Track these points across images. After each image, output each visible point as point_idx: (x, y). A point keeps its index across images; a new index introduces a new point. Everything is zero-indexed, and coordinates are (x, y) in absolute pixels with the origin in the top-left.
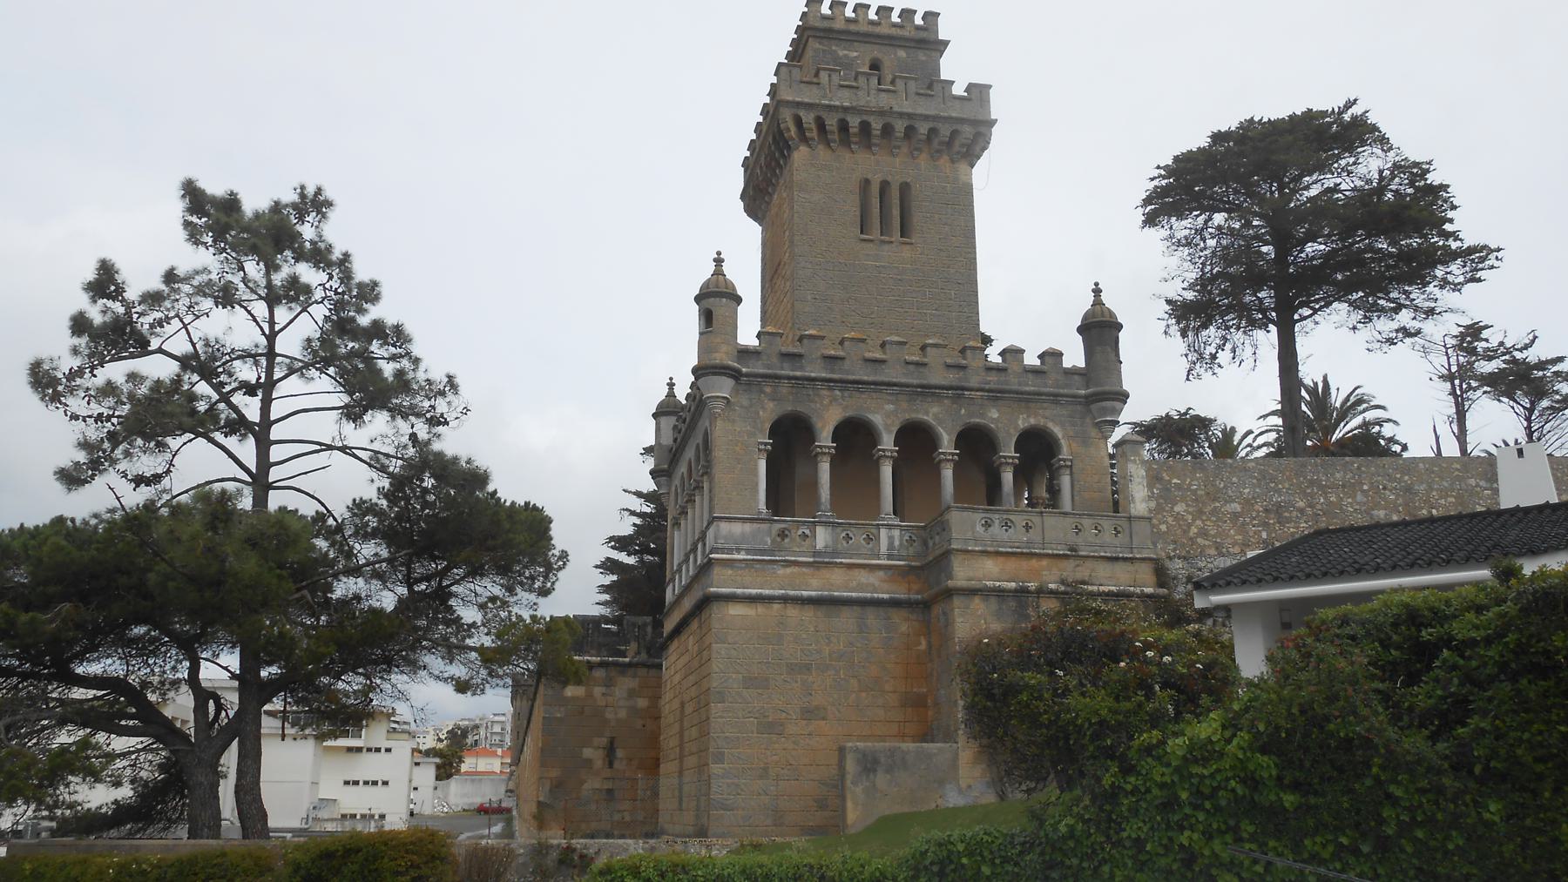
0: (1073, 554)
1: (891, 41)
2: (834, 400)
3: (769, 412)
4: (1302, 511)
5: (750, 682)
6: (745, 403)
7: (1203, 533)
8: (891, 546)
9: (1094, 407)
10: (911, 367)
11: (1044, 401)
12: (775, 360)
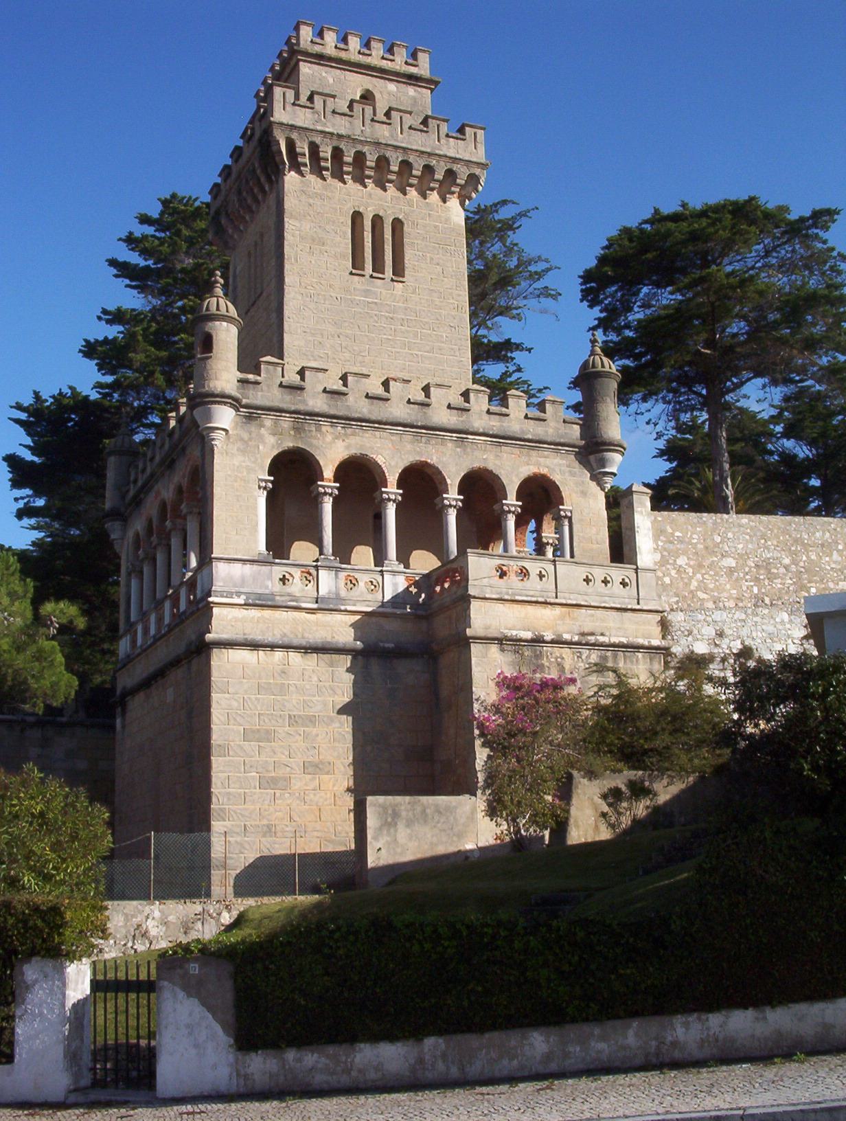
4: (786, 567)
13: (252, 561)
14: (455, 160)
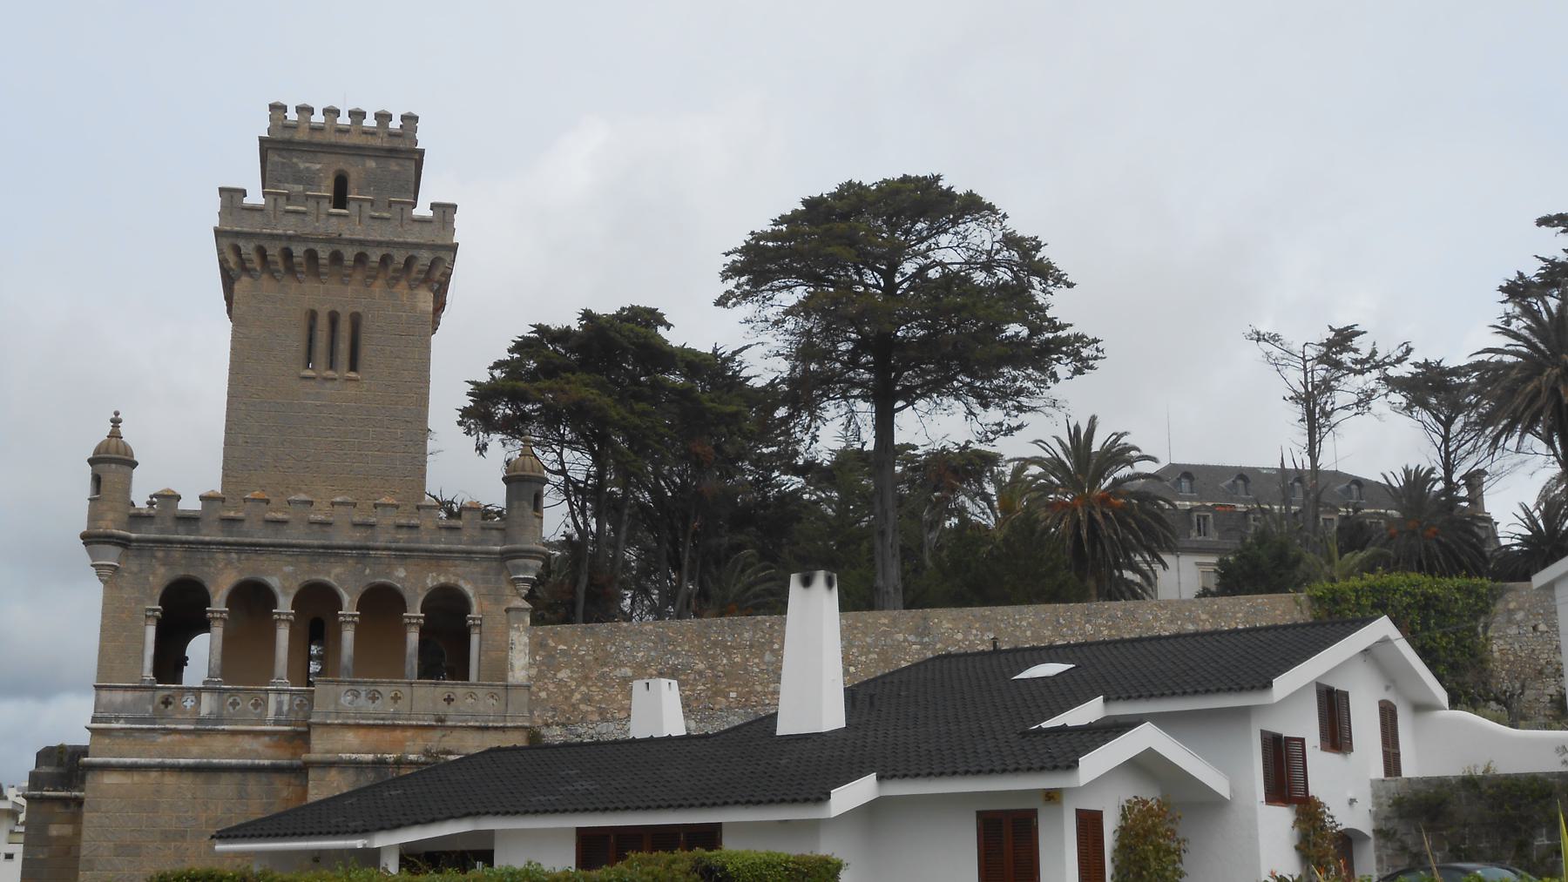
0: (440, 724)
1: (359, 151)
2: (229, 563)
3: (159, 576)
4: (700, 673)
5: (122, 850)
6: (135, 569)
7: (587, 699)
8: (279, 712)
9: (509, 563)
10: (316, 527)
11: (456, 559)
12: (169, 524)
13: (134, 688)
14: (389, 244)
